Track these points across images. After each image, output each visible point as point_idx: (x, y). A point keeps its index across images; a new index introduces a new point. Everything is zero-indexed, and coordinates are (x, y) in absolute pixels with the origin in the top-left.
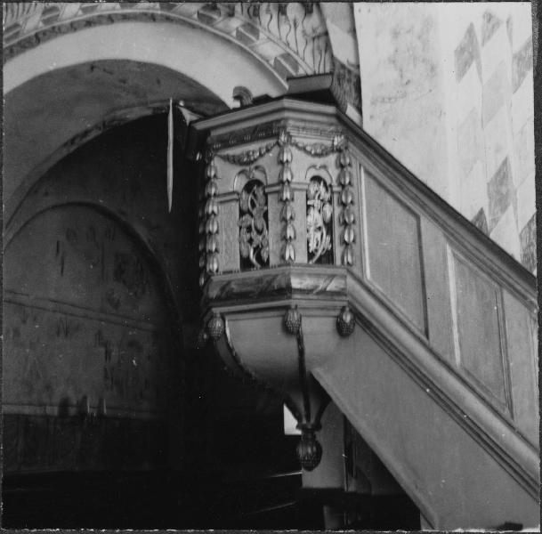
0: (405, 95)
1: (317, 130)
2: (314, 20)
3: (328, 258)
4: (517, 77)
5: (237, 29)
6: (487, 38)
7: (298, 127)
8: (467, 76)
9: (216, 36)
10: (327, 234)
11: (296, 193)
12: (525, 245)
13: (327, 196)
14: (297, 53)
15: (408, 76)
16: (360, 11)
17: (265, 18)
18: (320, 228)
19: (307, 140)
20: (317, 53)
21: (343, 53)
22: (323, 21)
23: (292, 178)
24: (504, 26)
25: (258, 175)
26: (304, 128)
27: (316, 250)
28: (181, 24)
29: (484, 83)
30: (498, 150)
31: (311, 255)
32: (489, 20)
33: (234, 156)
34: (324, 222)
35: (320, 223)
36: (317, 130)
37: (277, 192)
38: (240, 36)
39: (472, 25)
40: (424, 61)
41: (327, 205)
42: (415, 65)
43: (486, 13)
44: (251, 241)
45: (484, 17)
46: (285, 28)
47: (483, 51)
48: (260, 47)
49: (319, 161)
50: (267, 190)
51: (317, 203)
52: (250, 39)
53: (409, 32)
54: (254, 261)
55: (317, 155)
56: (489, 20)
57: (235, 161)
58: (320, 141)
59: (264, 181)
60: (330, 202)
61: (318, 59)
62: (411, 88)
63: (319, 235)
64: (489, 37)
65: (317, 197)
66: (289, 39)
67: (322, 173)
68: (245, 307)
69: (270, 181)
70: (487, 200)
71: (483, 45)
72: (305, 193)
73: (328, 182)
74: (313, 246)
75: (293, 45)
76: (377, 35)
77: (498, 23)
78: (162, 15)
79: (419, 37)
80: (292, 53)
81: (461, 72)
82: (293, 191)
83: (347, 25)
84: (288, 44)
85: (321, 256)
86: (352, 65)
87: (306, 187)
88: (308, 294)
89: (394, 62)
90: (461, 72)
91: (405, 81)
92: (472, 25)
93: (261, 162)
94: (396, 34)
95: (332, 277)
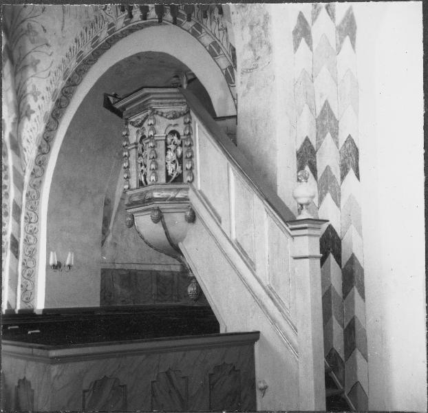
1: (170, 103)
3: (179, 179)
6: (314, 19)
7: (158, 103)
8: (298, 50)
10: (179, 164)
11: (159, 142)
12: (342, 158)
13: (179, 142)
15: (258, 54)
18: (174, 161)
19: (166, 109)
26: (161, 103)
27: (172, 175)
31: (168, 178)
34: (177, 157)
35: (174, 158)
39: (301, 12)
41: (179, 147)
42: (261, 46)
44: (142, 171)
46: (214, 24)
49: (173, 122)
51: (172, 147)
53: (257, 24)
54: (144, 182)
55: (170, 119)
58: (171, 110)
60: (181, 145)
62: (260, 62)
63: (174, 166)
64: (316, 18)
67: (176, 129)
68: (143, 208)
70: (314, 130)
71: (312, 24)
72: (164, 142)
74: (170, 172)
85: (176, 178)
88: (165, 200)
91: (257, 58)
94: (252, 27)
95: (179, 190)
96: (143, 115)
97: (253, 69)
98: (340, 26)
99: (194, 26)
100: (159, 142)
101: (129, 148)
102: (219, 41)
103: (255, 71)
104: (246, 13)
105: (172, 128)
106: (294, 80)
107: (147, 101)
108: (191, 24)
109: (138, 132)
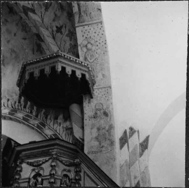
0: (101, 151)
2: (68, 124)
4: (141, 152)
5: (37, 124)
6: (131, 136)
8: (123, 149)
9: (28, 126)
14: (59, 134)
15: (103, 144)
16: (86, 120)
17: (49, 121)
20: (67, 135)
21: (77, 134)
22: (71, 124)
23: (56, 173)
24: (137, 132)
25: (41, 172)
28: (15, 121)
29: (130, 151)
30: (135, 178)
32: (131, 130)
33: (31, 162)
36: (68, 155)
37: (48, 179)
38: (38, 127)
39: (126, 130)
40: (109, 139)
42: (105, 141)
43: (130, 127)
45: (130, 129)
47: (129, 140)
48: (45, 131)
49: (67, 168)
50: (43, 178)
52: (42, 128)
56: (131, 130)
57: (31, 164)
59: (43, 175)
61: (67, 137)
62: (103, 149)
65: (65, 184)
66: (57, 129)
67: (68, 174)
69: (45, 174)
71: (129, 138)
73: (71, 178)
75: (58, 131)
76: (92, 129)
77: (135, 131)
78: (8, 117)
79: (107, 131)
80: (57, 134)
81: (121, 147)
82: (55, 179)
83: (80, 125)
84: (56, 131)
86: (81, 139)
87: (61, 178)
89: (97, 139)
90: (121, 147)
92: (126, 130)
93: (43, 166)
94: (99, 129)
96: (45, 158)
97: (97, 152)
98: (142, 143)
99: (39, 123)
100: (57, 180)
101: (20, 181)
102: (59, 134)
103: (99, 154)
104: (96, 122)
105: (65, 173)
106: (120, 164)
107: (51, 149)
108: (36, 122)
109: (33, 170)
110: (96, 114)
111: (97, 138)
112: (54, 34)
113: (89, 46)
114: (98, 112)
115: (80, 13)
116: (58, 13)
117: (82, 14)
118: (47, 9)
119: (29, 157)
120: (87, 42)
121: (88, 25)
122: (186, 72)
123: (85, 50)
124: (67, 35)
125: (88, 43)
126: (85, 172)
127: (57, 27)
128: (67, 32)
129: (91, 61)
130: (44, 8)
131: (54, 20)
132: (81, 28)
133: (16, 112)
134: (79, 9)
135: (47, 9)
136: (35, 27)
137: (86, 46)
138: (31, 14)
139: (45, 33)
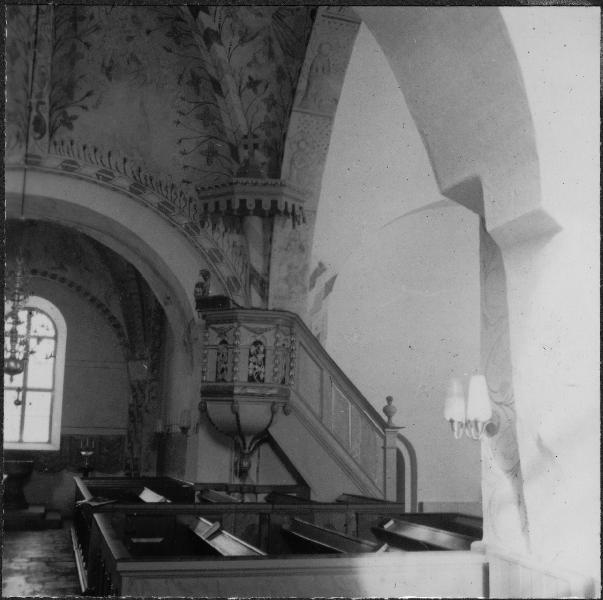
0: (290, 298)
94: (290, 267)
110: (289, 245)
111: (286, 280)
112: (242, 87)
113: (302, 145)
114: (293, 243)
115: (306, 96)
116: (262, 59)
117: (309, 96)
118: (242, 41)
119: (251, 320)
120: (300, 138)
121: (312, 115)
122: (599, 554)
123: (294, 146)
124: (265, 100)
125: (303, 140)
126: (301, 344)
127: (250, 78)
128: (266, 95)
129: (299, 167)
130: (237, 38)
131: (249, 65)
132: (300, 115)
133: (144, 190)
134: (307, 90)
135: (242, 41)
136: (215, 67)
137: (298, 143)
138: (202, 15)
139: (230, 83)
